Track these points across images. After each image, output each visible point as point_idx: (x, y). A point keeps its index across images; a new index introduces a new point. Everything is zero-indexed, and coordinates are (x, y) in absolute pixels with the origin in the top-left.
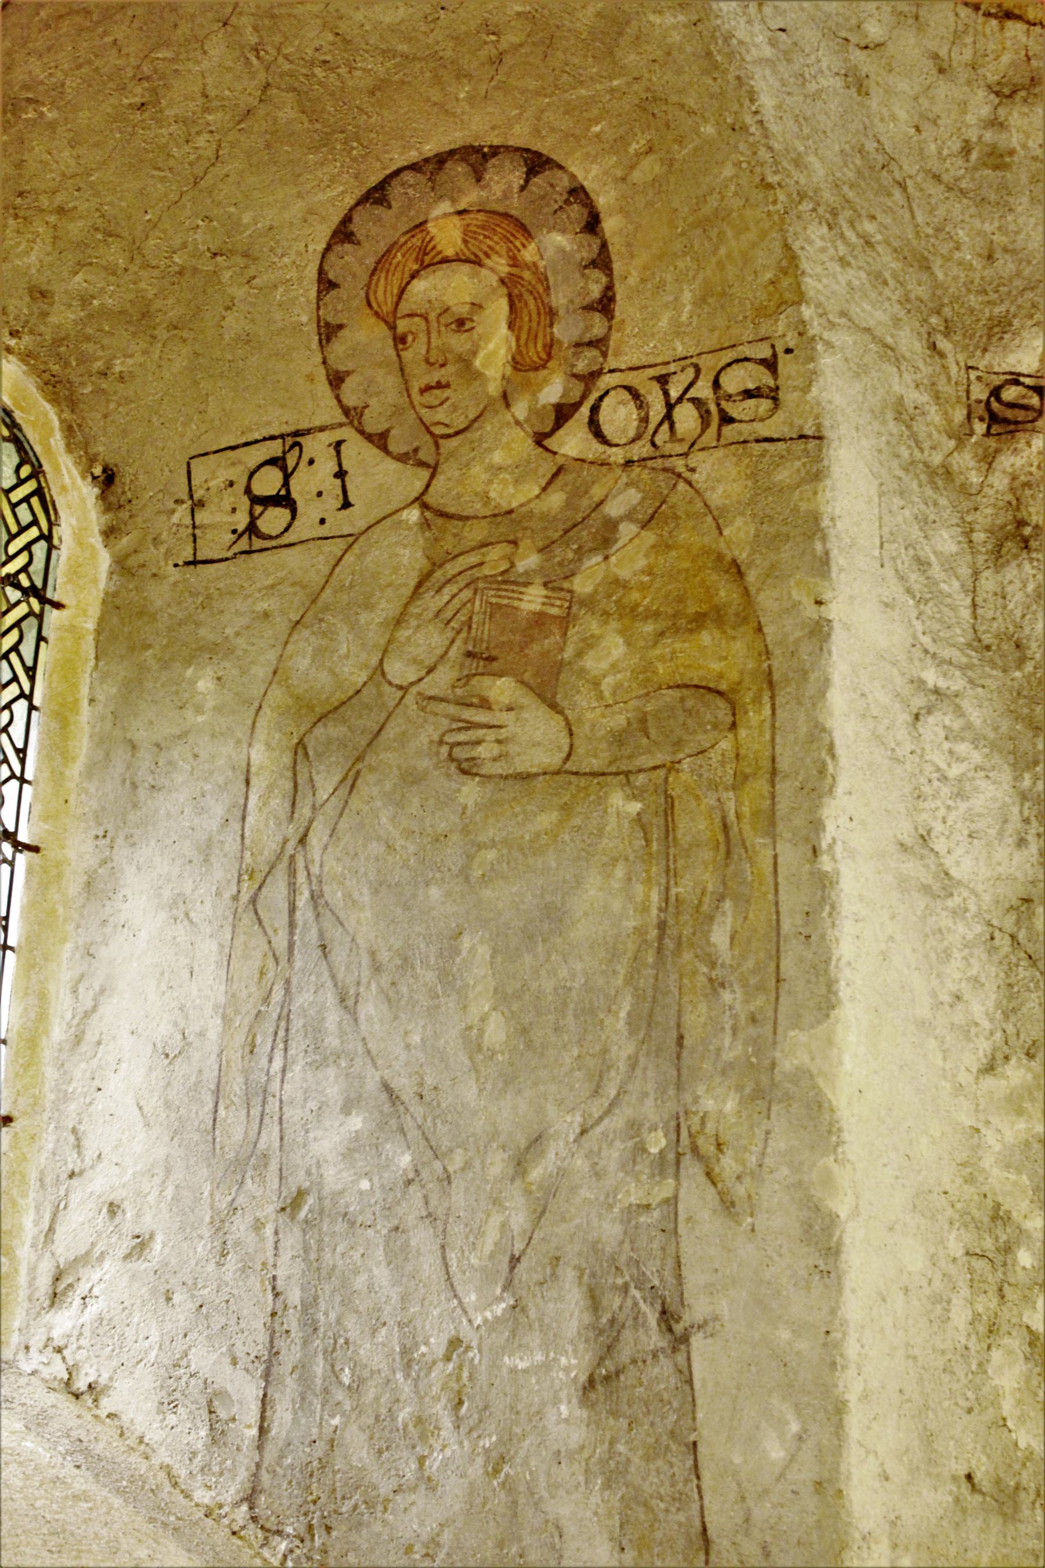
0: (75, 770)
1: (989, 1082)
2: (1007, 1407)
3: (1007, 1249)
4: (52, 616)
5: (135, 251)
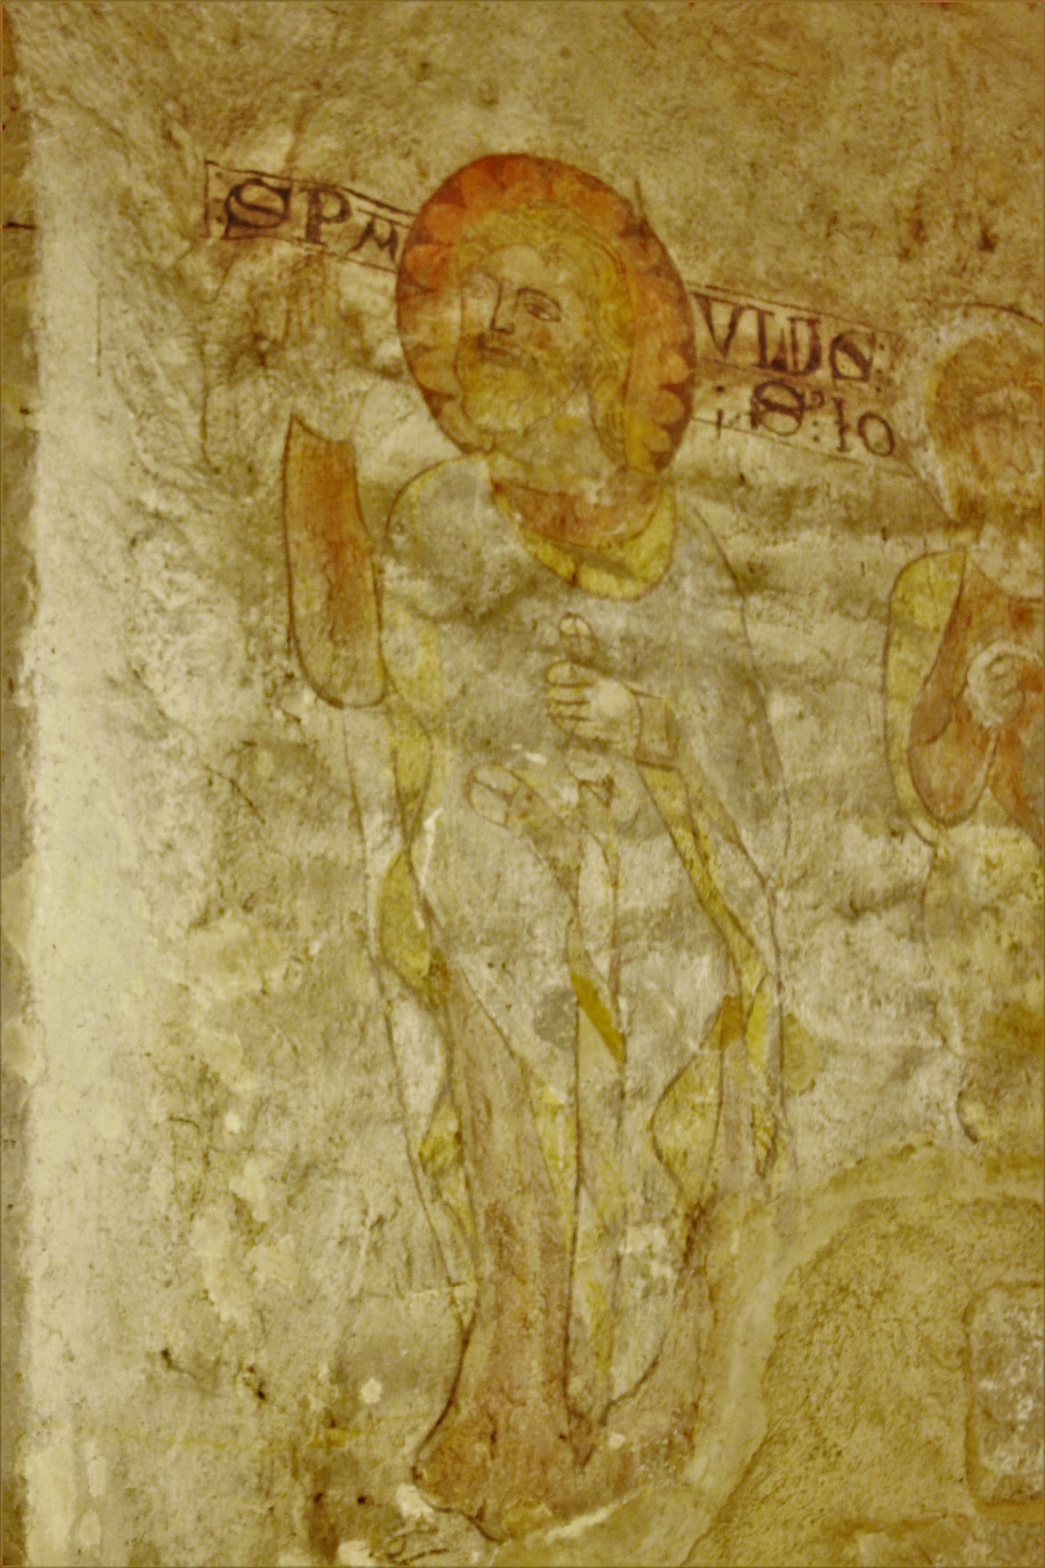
1: (201, 937)
2: (210, 1279)
3: (214, 1113)
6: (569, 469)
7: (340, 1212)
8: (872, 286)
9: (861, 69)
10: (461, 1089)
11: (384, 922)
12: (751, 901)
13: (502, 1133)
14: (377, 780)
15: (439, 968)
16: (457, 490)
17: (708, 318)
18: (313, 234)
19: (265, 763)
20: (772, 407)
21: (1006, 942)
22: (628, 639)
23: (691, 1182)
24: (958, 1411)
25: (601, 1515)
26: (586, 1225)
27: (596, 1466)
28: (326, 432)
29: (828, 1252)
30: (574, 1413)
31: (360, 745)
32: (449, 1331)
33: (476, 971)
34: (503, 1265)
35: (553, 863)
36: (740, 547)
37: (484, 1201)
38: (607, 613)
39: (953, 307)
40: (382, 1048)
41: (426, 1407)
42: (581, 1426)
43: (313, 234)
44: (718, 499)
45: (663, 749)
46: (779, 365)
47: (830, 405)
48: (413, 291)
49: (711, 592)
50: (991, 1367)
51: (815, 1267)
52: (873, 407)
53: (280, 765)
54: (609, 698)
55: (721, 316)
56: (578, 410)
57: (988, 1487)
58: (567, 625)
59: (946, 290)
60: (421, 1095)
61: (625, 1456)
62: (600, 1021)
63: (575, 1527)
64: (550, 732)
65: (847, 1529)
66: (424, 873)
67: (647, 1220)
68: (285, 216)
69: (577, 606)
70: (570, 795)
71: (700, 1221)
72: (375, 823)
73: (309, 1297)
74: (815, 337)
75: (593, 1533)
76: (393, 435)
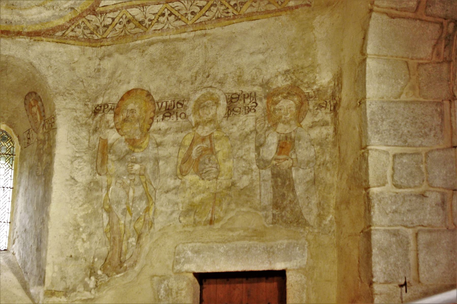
0: (17, 177)
1: (81, 208)
2: (79, 247)
3: (79, 229)
4: (14, 156)
5: (8, 110)
6: (134, 135)
7: (95, 238)
8: (185, 91)
9: (189, 53)
10: (110, 223)
11: (104, 203)
12: (152, 192)
13: (115, 228)
14: (105, 184)
15: (110, 207)
16: (120, 142)
17: (158, 105)
18: (103, 111)
19: (92, 184)
20: (166, 116)
21: (192, 192)
22: (141, 158)
23: (138, 233)
24: (172, 261)
25: (122, 274)
26: (125, 238)
27: (122, 268)
28: (104, 138)
29: (157, 240)
30: (121, 262)
31: (103, 180)
32: (107, 253)
33: (114, 207)
34: (114, 244)
35: (126, 191)
36: (159, 140)
37: (112, 236)
38: (138, 155)
39: (199, 90)
40: (101, 219)
41: (102, 262)
42: (121, 263)
43: (103, 111)
44: (156, 134)
45: (143, 173)
46: (168, 109)
47: (175, 113)
48: (116, 115)
49: (153, 148)
50: (178, 254)
51: (155, 242)
52: (183, 111)
53: (94, 184)
54: (137, 167)
55: (160, 104)
56: (137, 125)
57: (175, 271)
58: (132, 158)
59: (198, 87)
60: (106, 223)
61: (126, 267)
62: (129, 212)
63: (119, 275)
64: (127, 173)
65: (153, 276)
66: (109, 195)
67: (133, 237)
68: (100, 110)
69: (135, 154)
70: (129, 182)
71: (139, 237)
72: (104, 190)
73: (91, 248)
74: (174, 103)
75: (121, 276)
76: (112, 136)
